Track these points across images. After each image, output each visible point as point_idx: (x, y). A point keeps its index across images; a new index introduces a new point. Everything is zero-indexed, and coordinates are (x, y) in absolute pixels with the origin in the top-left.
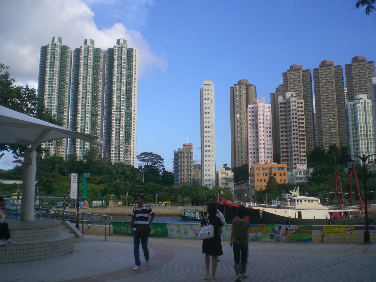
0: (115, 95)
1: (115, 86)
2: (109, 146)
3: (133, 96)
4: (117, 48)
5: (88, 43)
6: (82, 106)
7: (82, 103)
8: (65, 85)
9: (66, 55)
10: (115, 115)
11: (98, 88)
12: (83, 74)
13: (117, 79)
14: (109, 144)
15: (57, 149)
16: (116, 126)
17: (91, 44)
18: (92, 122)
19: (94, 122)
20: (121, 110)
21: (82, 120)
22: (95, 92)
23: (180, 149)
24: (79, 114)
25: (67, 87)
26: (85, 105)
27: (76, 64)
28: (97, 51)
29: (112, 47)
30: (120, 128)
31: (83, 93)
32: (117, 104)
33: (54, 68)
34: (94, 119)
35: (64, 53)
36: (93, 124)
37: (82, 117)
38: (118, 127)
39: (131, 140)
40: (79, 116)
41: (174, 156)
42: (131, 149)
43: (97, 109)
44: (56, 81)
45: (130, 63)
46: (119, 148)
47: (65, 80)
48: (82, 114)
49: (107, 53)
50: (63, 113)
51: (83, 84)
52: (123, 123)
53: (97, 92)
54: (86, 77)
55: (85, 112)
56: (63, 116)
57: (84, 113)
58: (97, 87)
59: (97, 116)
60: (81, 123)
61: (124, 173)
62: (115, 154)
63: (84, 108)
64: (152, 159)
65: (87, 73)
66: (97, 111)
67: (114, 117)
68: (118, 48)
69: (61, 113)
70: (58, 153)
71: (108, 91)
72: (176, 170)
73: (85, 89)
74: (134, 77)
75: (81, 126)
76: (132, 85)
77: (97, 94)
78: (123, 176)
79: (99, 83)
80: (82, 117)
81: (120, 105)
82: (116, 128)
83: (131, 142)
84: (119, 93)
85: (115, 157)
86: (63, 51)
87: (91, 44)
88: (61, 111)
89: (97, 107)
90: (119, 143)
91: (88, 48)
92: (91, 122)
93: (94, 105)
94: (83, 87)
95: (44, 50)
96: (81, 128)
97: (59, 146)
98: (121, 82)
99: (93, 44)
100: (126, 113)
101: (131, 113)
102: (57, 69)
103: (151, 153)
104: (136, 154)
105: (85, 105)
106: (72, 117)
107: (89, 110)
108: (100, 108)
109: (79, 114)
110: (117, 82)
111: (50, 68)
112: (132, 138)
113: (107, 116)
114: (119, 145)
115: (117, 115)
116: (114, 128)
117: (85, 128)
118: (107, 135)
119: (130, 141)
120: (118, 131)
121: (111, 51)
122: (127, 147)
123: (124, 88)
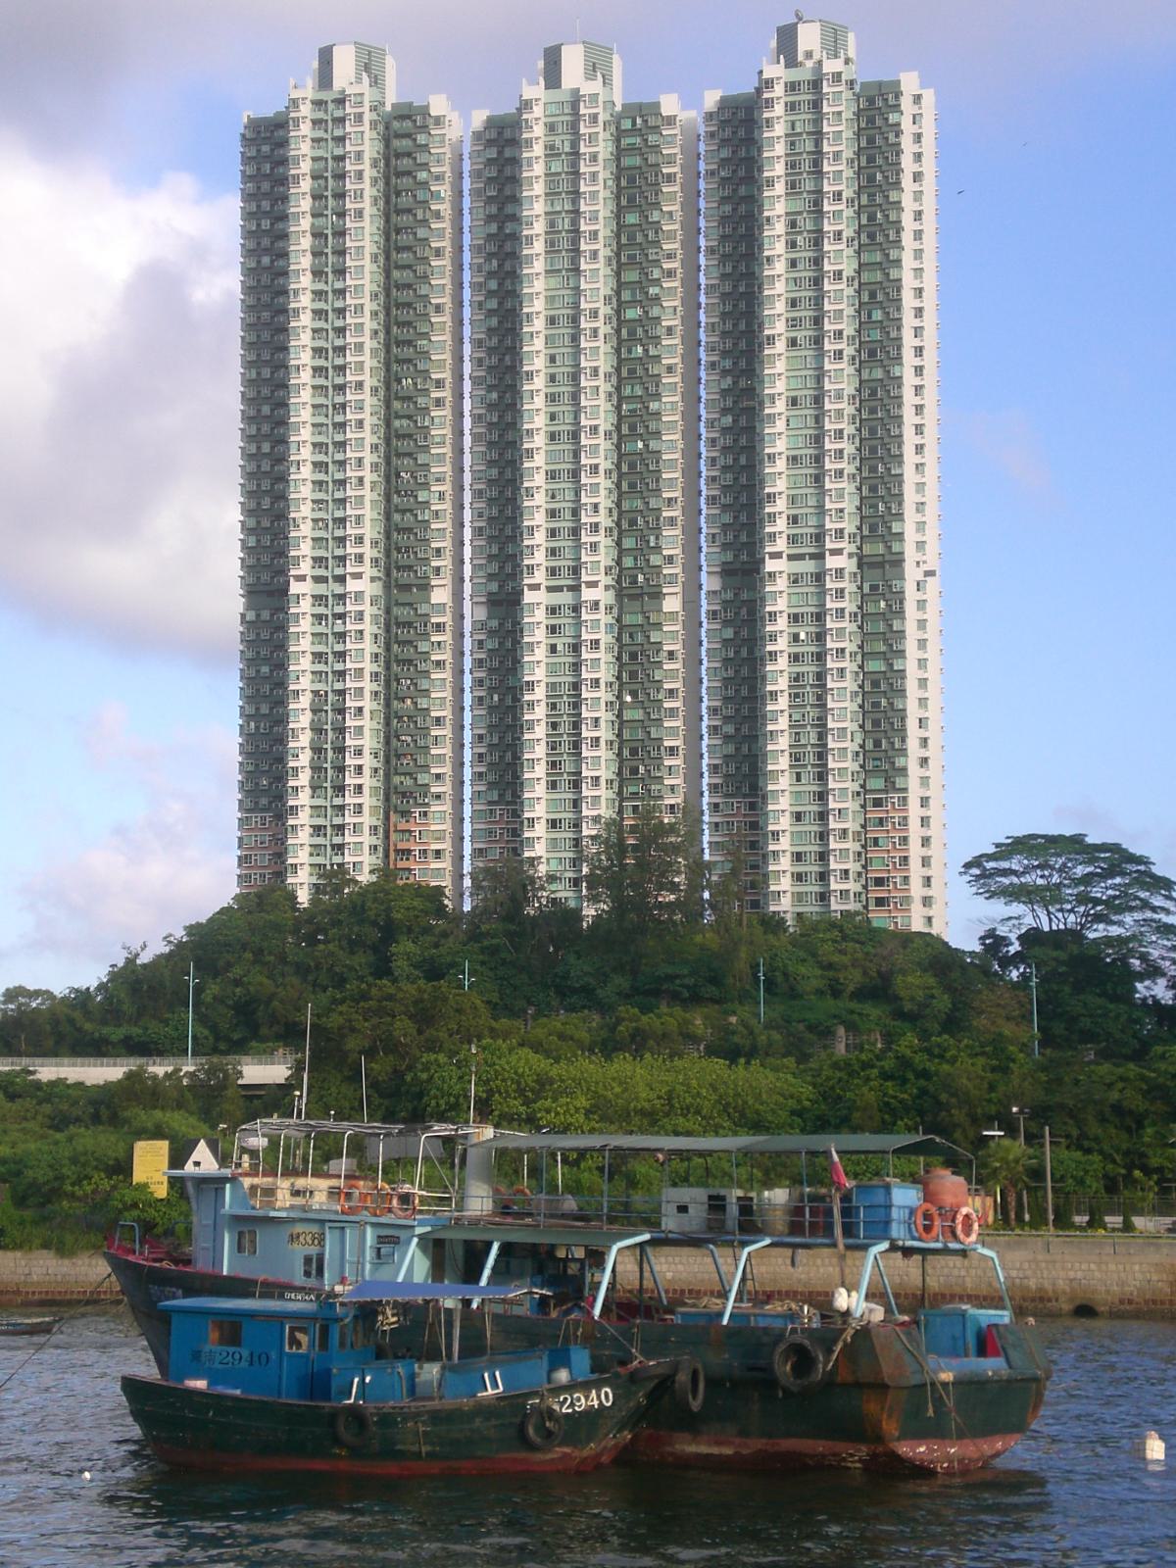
0: (780, 439)
1: (780, 375)
2: (752, 806)
3: (910, 439)
6: (553, 533)
7: (552, 514)
8: (426, 392)
10: (782, 584)
11: (657, 396)
12: (550, 300)
13: (793, 323)
14: (746, 790)
15: (393, 837)
16: (795, 658)
18: (626, 639)
19: (639, 638)
20: (829, 545)
21: (553, 630)
22: (632, 428)
24: (535, 587)
25: (439, 402)
26: (570, 527)
27: (490, 237)
30: (820, 676)
31: (553, 437)
32: (793, 500)
33: (341, 272)
36: (633, 656)
37: (553, 610)
38: (809, 669)
39: (903, 752)
40: (536, 601)
43: (658, 549)
46: (823, 816)
47: (425, 355)
48: (550, 589)
50: (426, 588)
51: (552, 378)
52: (843, 635)
53: (653, 426)
54: (569, 322)
55: (576, 571)
56: (423, 609)
57: (571, 578)
58: (652, 390)
59: (657, 596)
60: (553, 649)
61: (878, 990)
62: (798, 857)
63: (564, 543)
65: (577, 291)
66: (655, 560)
67: (780, 599)
69: (407, 588)
73: (564, 408)
74: (908, 300)
75: (552, 670)
76: (898, 359)
77: (653, 445)
78: (874, 1011)
79: (658, 357)
80: (553, 610)
81: (821, 510)
82: (797, 677)
83: (903, 771)
84: (811, 422)
85: (799, 877)
88: (405, 577)
89: (657, 530)
90: (822, 777)
93: (633, 522)
94: (552, 398)
96: (552, 686)
97: (405, 814)
98: (818, 341)
101: (898, 562)
105: (570, 527)
106: (482, 614)
107: (599, 557)
108: (672, 541)
109: (777, 555)
110: (793, 343)
111: (318, 274)
112: (912, 744)
113: (729, 595)
114: (822, 796)
115: (795, 579)
116: (779, 676)
117: (576, 686)
119: (900, 762)
120: (813, 691)
122: (878, 803)
123: (842, 379)
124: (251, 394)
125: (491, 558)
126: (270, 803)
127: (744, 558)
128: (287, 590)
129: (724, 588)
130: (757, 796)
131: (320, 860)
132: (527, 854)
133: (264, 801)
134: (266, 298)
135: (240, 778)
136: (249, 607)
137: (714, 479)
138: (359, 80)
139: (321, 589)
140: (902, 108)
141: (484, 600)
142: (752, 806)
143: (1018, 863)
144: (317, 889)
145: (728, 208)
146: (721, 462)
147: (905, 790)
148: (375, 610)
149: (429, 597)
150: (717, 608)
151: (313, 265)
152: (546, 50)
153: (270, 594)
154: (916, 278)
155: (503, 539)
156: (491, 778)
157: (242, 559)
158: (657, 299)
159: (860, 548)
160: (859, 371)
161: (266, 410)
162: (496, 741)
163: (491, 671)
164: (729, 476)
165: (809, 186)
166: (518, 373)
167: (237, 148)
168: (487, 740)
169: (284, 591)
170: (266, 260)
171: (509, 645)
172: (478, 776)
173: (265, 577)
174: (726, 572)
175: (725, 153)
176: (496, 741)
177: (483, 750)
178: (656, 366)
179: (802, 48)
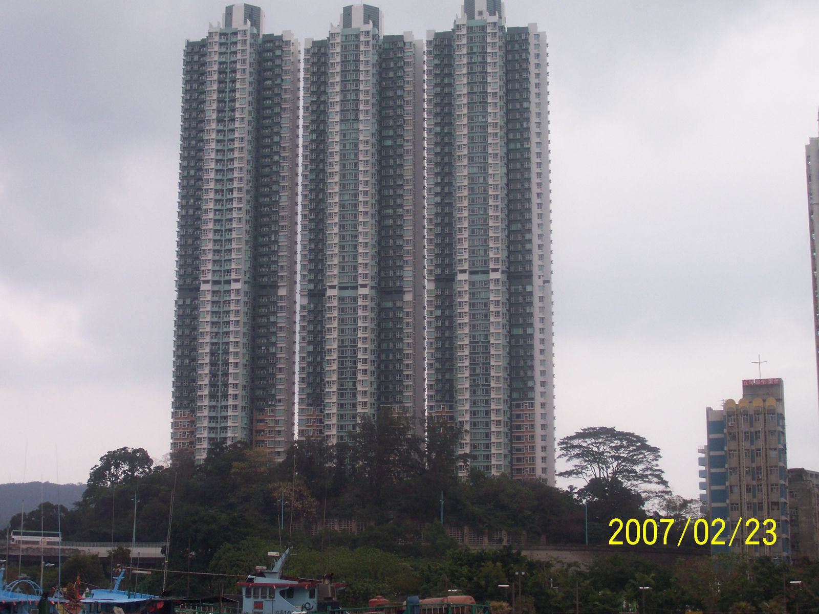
2: (451, 407)
4: (464, 31)
5: (357, 21)
9: (276, 158)
14: (447, 398)
17: (366, 22)
23: (731, 402)
27: (313, 102)
28: (393, 51)
29: (448, 27)
34: (390, 305)
35: (270, 64)
41: (709, 433)
42: (533, 459)
44: (240, 231)
45: (517, 57)
49: (429, 52)
64: (617, 448)
68: (470, 29)
70: (259, 438)
71: (437, 307)
72: (713, 470)
86: (261, 200)
87: (366, 22)
91: (357, 36)
92: (379, 356)
95: (192, 153)
97: (262, 410)
99: (376, 24)
100: (508, 278)
102: (242, 129)
103: (612, 430)
104: (558, 440)
106: (305, 301)
113: (439, 292)
118: (438, 365)
121: (442, 45)
124: (184, 213)
125: (310, 261)
126: (189, 404)
127: (447, 272)
128: (199, 288)
129: (436, 288)
130: (453, 402)
131: (213, 435)
132: (327, 412)
133: (185, 402)
134: (189, 261)
135: (175, 319)
136: (179, 297)
137: (431, 230)
138: (245, 22)
139: (216, 288)
140: (531, 100)
141: (306, 293)
142: (451, 407)
143: (595, 441)
144: (210, 452)
145: (438, 89)
146: (434, 221)
147: (533, 399)
148: (244, 393)
149: (277, 292)
150: (433, 383)
151: (218, 88)
152: (344, 8)
153: (191, 290)
154: (536, 107)
155: (317, 221)
156: (309, 391)
157: (179, 212)
158: (401, 186)
159: (509, 268)
160: (507, 134)
161: (192, 172)
162: (311, 370)
163: (309, 332)
164: (439, 229)
165: (481, 360)
166: (326, 163)
167: (181, 56)
168: (307, 370)
169: (198, 289)
170: (194, 114)
171: (319, 359)
172: (302, 380)
173: (188, 281)
174: (438, 280)
175: (437, 62)
176: (311, 370)
177: (304, 376)
178: (401, 344)
179: (477, 9)
